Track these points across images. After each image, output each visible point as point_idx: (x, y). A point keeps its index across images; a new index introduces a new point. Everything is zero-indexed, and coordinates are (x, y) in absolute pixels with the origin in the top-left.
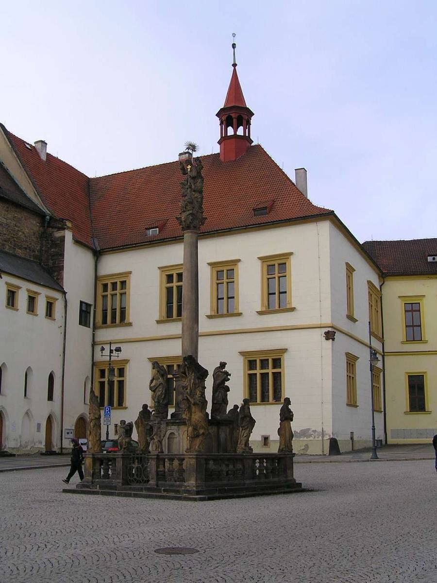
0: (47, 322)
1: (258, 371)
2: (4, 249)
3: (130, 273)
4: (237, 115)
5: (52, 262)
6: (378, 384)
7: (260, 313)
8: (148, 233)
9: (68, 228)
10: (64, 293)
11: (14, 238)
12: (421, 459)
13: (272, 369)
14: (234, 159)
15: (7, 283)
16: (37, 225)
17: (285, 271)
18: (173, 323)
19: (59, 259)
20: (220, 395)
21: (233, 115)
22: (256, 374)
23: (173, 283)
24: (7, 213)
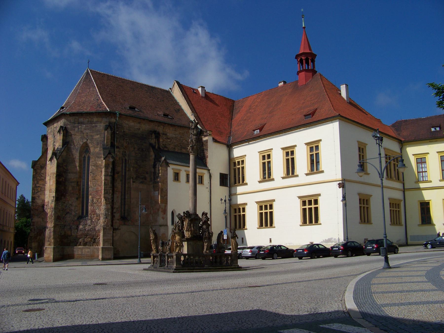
1: (307, 207)
2: (175, 150)
4: (305, 57)
10: (209, 170)
12: (404, 253)
14: (305, 84)
15: (172, 169)
21: (303, 58)
22: (306, 208)
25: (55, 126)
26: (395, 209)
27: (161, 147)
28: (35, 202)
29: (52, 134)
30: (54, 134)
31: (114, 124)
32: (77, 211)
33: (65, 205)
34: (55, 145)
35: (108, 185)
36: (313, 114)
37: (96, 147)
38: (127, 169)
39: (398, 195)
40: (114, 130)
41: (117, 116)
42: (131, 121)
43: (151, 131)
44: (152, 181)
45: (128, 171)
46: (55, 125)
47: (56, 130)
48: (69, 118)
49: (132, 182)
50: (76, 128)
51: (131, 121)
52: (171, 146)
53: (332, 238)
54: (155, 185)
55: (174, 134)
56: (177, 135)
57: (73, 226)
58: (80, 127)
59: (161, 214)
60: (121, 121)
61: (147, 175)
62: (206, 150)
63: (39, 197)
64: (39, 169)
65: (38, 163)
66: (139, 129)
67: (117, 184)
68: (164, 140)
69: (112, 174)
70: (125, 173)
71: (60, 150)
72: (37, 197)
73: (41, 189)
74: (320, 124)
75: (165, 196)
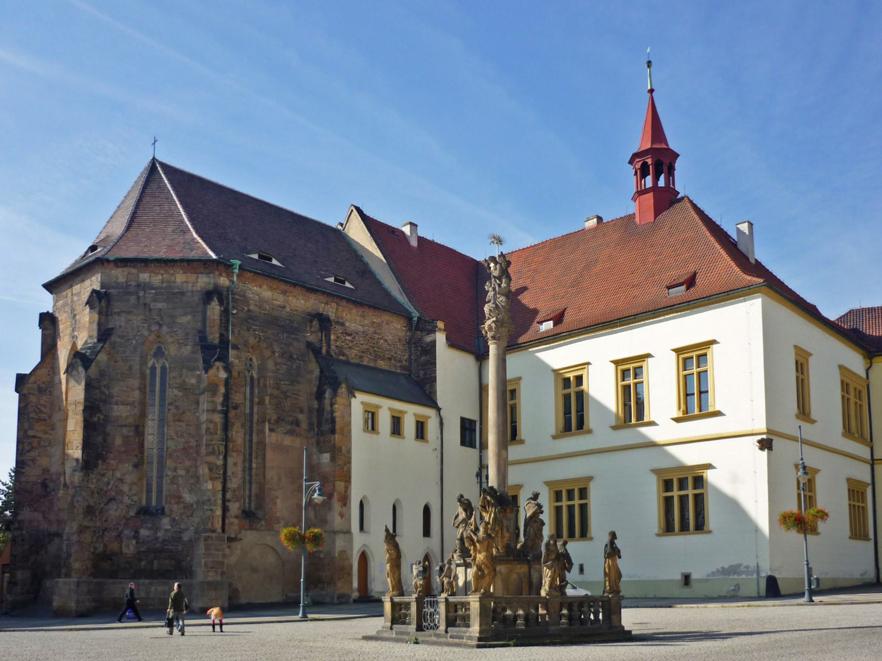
0: (419, 444)
2: (362, 362)
3: (520, 379)
5: (423, 372)
6: (863, 502)
7: (677, 420)
8: (541, 328)
9: (440, 330)
10: (439, 409)
11: (373, 347)
13: (678, 491)
15: (362, 403)
16: (403, 330)
17: (705, 365)
18: (580, 436)
19: (431, 368)
20: (531, 529)
21: (649, 161)
23: (570, 388)
24: (362, 319)
25: (74, 292)
26: (857, 504)
27: (332, 353)
28: (23, 473)
29: (67, 310)
30: (73, 310)
31: (225, 289)
32: (135, 495)
33: (107, 480)
34: (77, 337)
35: (216, 434)
36: (690, 282)
37: (182, 343)
38: (256, 400)
39: (862, 473)
40: (228, 304)
41: (233, 273)
42: (265, 287)
43: (310, 314)
44: (314, 430)
45: (259, 403)
46: (76, 288)
47: (79, 300)
48: (113, 271)
49: (267, 431)
50: (133, 297)
51: (265, 287)
52: (354, 351)
53: (740, 565)
54: (322, 438)
55: (360, 325)
56: (367, 328)
57: (126, 532)
58: (141, 295)
59: (337, 506)
60: (243, 284)
61: (301, 417)
62: (431, 365)
63: (33, 460)
64: (33, 394)
65: (32, 379)
66: (284, 307)
67: (234, 433)
68: (338, 337)
69: (224, 409)
70: (252, 408)
71: (90, 347)
72: (30, 460)
73: (39, 444)
74: (731, 299)
75: (345, 465)
